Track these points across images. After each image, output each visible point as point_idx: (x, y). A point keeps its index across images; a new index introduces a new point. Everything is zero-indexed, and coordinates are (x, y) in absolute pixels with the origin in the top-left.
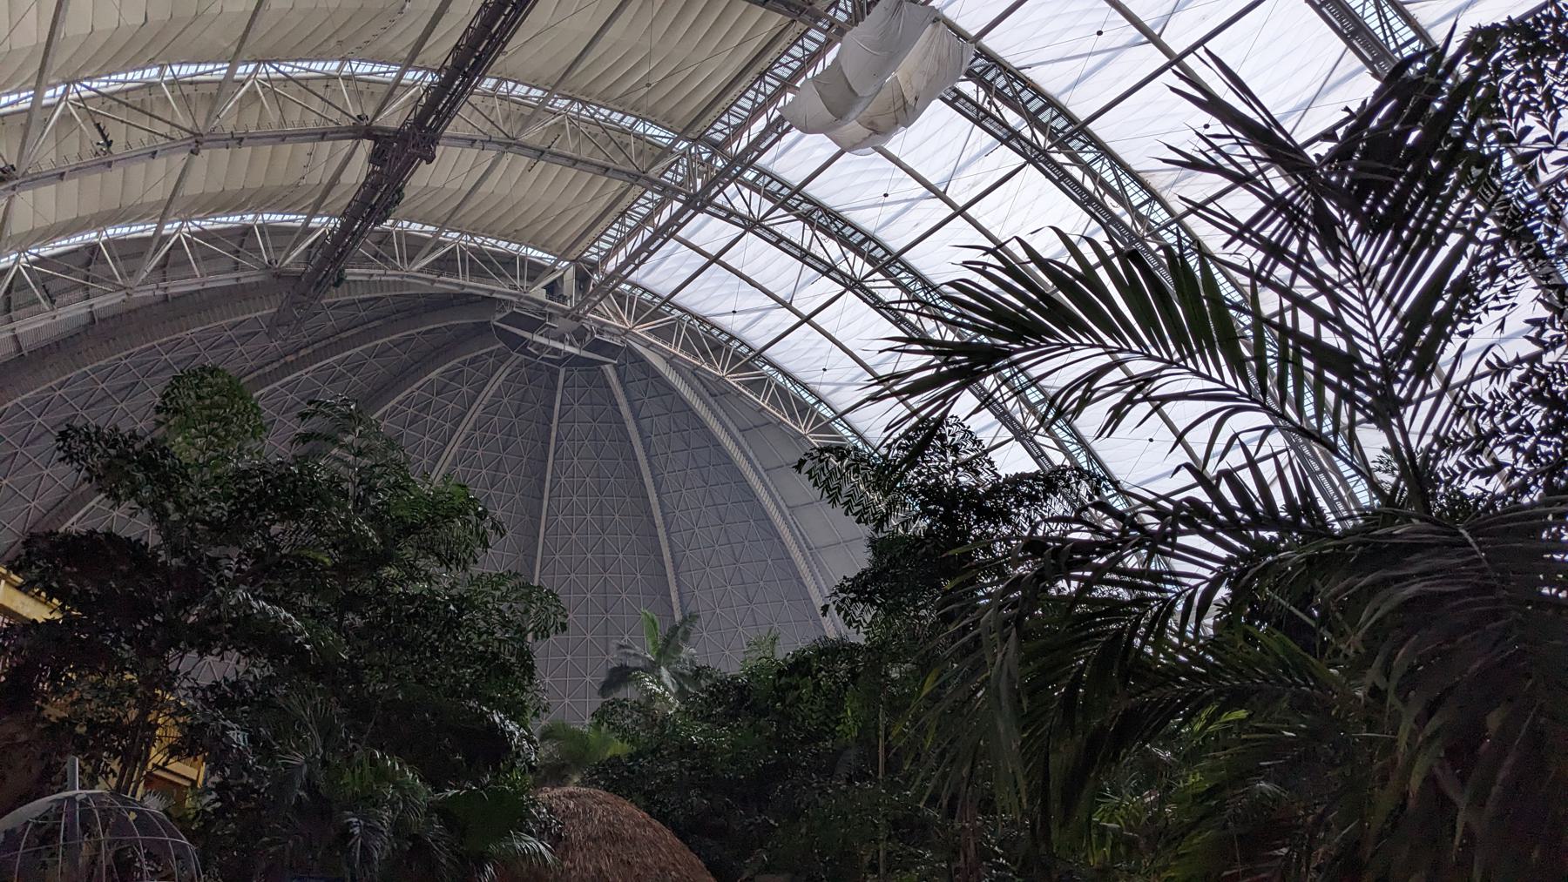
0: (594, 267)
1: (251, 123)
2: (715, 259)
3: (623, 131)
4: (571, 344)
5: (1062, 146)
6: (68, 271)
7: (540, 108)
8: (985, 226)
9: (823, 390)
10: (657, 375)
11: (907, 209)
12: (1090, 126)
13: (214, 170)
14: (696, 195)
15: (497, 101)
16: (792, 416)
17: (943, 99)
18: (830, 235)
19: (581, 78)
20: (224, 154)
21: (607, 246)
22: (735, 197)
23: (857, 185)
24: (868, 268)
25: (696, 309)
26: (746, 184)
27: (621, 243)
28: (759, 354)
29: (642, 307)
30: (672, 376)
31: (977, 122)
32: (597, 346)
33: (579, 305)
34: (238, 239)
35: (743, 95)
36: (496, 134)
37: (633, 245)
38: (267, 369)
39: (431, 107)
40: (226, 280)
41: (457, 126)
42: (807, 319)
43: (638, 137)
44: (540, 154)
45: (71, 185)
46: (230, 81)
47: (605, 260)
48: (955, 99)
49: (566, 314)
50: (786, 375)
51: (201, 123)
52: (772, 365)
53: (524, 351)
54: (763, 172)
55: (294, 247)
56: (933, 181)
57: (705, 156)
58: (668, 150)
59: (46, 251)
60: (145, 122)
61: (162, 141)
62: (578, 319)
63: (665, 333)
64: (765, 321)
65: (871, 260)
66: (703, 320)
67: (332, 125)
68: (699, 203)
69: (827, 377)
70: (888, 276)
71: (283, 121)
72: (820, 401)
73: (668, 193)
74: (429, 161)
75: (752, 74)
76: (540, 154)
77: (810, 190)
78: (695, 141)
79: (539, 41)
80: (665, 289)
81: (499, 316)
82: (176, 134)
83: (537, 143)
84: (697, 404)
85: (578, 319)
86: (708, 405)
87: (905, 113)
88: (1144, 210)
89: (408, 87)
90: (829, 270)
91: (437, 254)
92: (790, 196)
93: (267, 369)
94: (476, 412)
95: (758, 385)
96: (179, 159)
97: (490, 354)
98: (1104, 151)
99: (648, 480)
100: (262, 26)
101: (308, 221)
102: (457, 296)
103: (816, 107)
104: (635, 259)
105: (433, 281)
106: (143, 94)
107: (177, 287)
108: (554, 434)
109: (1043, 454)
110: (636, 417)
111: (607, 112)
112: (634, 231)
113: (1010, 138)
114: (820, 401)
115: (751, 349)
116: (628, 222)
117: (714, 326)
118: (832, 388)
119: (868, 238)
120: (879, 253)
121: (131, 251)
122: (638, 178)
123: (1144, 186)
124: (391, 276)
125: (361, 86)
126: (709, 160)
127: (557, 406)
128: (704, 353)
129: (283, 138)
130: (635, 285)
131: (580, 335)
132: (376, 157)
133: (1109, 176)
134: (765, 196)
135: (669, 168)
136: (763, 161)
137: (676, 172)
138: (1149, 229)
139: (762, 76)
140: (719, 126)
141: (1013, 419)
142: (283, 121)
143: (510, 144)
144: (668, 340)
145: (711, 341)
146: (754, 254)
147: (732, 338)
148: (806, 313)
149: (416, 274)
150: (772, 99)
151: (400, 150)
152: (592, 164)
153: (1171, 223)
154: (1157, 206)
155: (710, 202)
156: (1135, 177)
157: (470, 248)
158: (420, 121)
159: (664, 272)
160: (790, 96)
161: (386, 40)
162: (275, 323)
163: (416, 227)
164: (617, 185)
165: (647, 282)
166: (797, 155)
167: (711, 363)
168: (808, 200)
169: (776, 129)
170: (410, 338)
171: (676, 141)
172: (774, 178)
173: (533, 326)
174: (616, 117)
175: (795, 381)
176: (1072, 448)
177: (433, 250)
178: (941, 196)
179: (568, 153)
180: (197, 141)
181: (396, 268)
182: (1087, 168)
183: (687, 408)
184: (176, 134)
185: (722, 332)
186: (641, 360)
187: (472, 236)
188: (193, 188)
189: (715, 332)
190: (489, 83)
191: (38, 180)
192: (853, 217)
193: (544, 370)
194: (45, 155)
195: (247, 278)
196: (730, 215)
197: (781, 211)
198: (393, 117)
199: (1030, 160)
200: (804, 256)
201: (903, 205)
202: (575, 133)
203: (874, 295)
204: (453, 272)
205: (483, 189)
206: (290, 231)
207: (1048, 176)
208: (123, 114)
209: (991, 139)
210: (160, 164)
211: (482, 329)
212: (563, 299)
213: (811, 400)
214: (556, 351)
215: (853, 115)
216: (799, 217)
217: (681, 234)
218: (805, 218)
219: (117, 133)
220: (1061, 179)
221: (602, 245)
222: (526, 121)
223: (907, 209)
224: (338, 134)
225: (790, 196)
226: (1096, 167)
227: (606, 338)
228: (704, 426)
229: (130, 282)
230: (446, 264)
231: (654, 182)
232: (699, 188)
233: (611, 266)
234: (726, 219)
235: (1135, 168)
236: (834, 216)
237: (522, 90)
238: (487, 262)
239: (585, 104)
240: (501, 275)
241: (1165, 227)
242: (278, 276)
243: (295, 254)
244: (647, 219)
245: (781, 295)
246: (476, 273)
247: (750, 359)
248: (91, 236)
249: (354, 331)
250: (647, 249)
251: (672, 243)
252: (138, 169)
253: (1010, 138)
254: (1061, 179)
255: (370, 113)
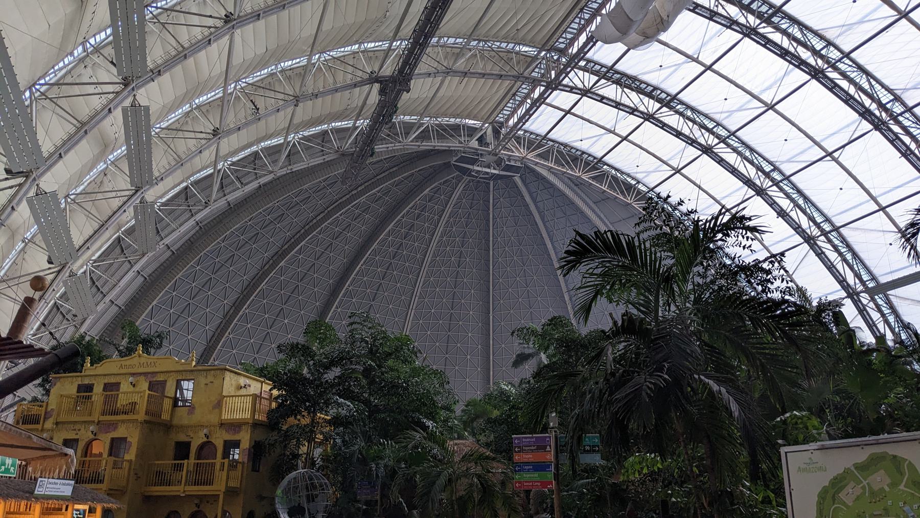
0: (501, 125)
1: (320, 87)
2: (568, 112)
3: (508, 52)
4: (494, 169)
5: (768, 21)
6: (245, 167)
7: (463, 50)
8: (725, 74)
9: (639, 176)
10: (544, 178)
11: (676, 70)
12: (784, 8)
13: (305, 110)
14: (552, 81)
15: (440, 49)
16: (622, 193)
17: (689, 10)
18: (632, 90)
19: (482, 31)
20: (310, 103)
21: (508, 113)
22: (578, 78)
23: (643, 62)
24: (658, 105)
25: (561, 140)
26: (580, 68)
27: (514, 111)
28: (600, 160)
29: (531, 143)
30: (551, 178)
31: (711, 19)
32: (509, 168)
33: (497, 147)
34: (321, 138)
35: (572, 22)
36: (440, 68)
37: (521, 111)
38: (344, 199)
39: (406, 63)
40: (318, 160)
41: (422, 68)
42: (709, 68)
43: (518, 53)
44: (465, 74)
45: (243, 132)
46: (310, 65)
47: (507, 120)
48: (695, 8)
49: (489, 153)
50: (616, 169)
51: (297, 90)
52: (608, 165)
53: (470, 175)
54: (589, 61)
55: (350, 136)
56: (690, 53)
57: (555, 58)
58: (535, 58)
59: (235, 159)
60: (272, 94)
61: (203, 142)
62: (496, 155)
63: (544, 156)
64: (599, 143)
65: (659, 100)
66: (565, 145)
67: (359, 79)
68: (554, 85)
69: (639, 169)
70: (671, 108)
71: (335, 82)
72: (638, 182)
73: (535, 83)
74: (408, 92)
75: (577, 10)
76: (465, 74)
77: (618, 67)
78: (549, 51)
79: (455, 19)
80: (543, 131)
81: (455, 159)
82: (287, 98)
83: (462, 69)
84: (568, 192)
85: (496, 155)
86: (572, 190)
87: (664, 24)
88: (823, 52)
89: (395, 50)
90: (633, 111)
91: (422, 129)
92: (608, 72)
93: (344, 199)
94: (449, 210)
95: (600, 178)
96: (290, 110)
97: (453, 178)
98: (794, 21)
99: (545, 235)
100: (321, 37)
101: (355, 123)
102: (432, 150)
103: (611, 30)
104: (523, 119)
105: (419, 146)
106: (270, 79)
107: (297, 167)
108: (491, 216)
109: (775, 202)
110: (534, 201)
111: (498, 44)
112: (522, 103)
113: (731, 25)
114: (638, 182)
115: (595, 158)
116: (517, 98)
117: (572, 148)
118: (838, 31)
119: (655, 88)
120: (663, 96)
121: (273, 151)
122: (518, 77)
123: (822, 38)
124: (398, 146)
125: (370, 54)
126: (558, 59)
127: (491, 201)
128: (568, 163)
129: (336, 90)
130: (526, 131)
131: (499, 163)
132: (382, 92)
133: (798, 35)
134: (592, 73)
135: (536, 67)
136: (589, 55)
137: (540, 68)
138: (828, 62)
139: (581, 10)
140: (561, 40)
141: (754, 184)
142: (335, 82)
143: (448, 72)
144: (547, 159)
145: (571, 157)
146: (588, 106)
147: (583, 153)
148: (624, 135)
149: (410, 143)
150: (589, 22)
151: (393, 86)
152: (493, 75)
153: (842, 58)
154: (832, 48)
155: (560, 84)
156: (816, 33)
157: (436, 125)
158: (401, 71)
159: (540, 122)
160: (599, 18)
161: (382, 28)
162: (345, 178)
163: (407, 118)
164: (507, 83)
165: (596, 58)
166: (605, 53)
167: (572, 169)
168: (617, 72)
169: (592, 40)
170: (413, 174)
171: (539, 53)
172: (596, 63)
173: (473, 162)
174: (504, 45)
175: (622, 173)
176: (794, 196)
177: (419, 128)
178: (696, 60)
179: (480, 71)
180: (297, 100)
181: (400, 142)
182: (784, 32)
183: (563, 194)
184: (287, 98)
185: (577, 150)
186: (533, 171)
187: (436, 118)
188: (296, 121)
189: (574, 151)
190: (435, 40)
191: (229, 132)
192: (645, 78)
193: (482, 184)
194: (231, 120)
195: (328, 158)
196: (572, 89)
197: (603, 81)
198: (388, 70)
199: (745, 35)
200: (618, 105)
201: (673, 68)
202: (483, 57)
203: (765, 37)
204: (429, 138)
205: (440, 94)
206: (347, 129)
207: (758, 43)
208: (261, 92)
209: (720, 26)
210: (281, 113)
211: (447, 165)
212: (487, 145)
213: (633, 182)
214: (487, 173)
215: (632, 31)
216: (614, 82)
217: (548, 101)
218: (617, 82)
219: (260, 103)
220: (766, 43)
221: (505, 112)
222: (457, 56)
223: (676, 70)
224: (362, 83)
225: (608, 72)
226: (790, 31)
227: (512, 163)
228: (573, 203)
229: (276, 169)
230: (425, 135)
231: (527, 78)
232: (553, 76)
233: (511, 123)
234: (570, 91)
235: (815, 28)
236: (634, 79)
237: (452, 40)
238: (445, 130)
239: (486, 41)
240: (452, 136)
241: (840, 60)
242: (343, 155)
243: (350, 142)
244: (527, 96)
245: (608, 126)
246: (441, 137)
247: (595, 164)
248: (254, 148)
249: (383, 175)
250: (528, 114)
251: (543, 106)
252: (272, 119)
253: (731, 25)
254: (766, 43)
255: (376, 70)
